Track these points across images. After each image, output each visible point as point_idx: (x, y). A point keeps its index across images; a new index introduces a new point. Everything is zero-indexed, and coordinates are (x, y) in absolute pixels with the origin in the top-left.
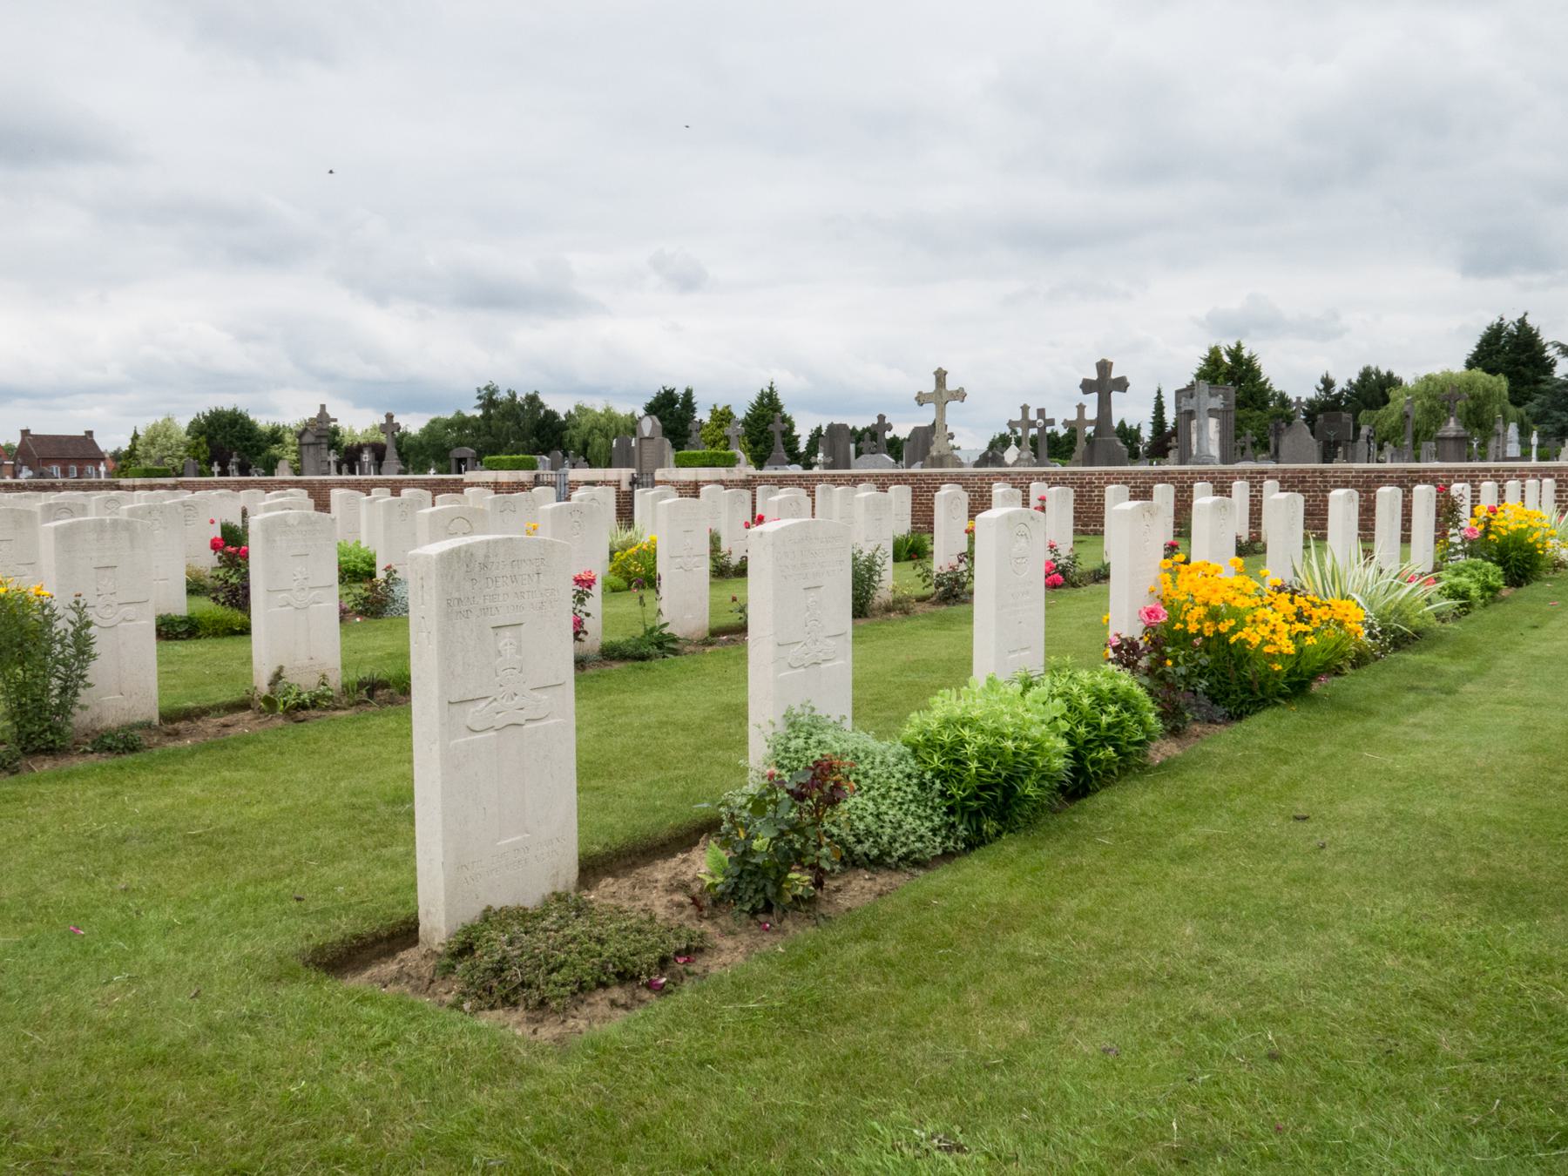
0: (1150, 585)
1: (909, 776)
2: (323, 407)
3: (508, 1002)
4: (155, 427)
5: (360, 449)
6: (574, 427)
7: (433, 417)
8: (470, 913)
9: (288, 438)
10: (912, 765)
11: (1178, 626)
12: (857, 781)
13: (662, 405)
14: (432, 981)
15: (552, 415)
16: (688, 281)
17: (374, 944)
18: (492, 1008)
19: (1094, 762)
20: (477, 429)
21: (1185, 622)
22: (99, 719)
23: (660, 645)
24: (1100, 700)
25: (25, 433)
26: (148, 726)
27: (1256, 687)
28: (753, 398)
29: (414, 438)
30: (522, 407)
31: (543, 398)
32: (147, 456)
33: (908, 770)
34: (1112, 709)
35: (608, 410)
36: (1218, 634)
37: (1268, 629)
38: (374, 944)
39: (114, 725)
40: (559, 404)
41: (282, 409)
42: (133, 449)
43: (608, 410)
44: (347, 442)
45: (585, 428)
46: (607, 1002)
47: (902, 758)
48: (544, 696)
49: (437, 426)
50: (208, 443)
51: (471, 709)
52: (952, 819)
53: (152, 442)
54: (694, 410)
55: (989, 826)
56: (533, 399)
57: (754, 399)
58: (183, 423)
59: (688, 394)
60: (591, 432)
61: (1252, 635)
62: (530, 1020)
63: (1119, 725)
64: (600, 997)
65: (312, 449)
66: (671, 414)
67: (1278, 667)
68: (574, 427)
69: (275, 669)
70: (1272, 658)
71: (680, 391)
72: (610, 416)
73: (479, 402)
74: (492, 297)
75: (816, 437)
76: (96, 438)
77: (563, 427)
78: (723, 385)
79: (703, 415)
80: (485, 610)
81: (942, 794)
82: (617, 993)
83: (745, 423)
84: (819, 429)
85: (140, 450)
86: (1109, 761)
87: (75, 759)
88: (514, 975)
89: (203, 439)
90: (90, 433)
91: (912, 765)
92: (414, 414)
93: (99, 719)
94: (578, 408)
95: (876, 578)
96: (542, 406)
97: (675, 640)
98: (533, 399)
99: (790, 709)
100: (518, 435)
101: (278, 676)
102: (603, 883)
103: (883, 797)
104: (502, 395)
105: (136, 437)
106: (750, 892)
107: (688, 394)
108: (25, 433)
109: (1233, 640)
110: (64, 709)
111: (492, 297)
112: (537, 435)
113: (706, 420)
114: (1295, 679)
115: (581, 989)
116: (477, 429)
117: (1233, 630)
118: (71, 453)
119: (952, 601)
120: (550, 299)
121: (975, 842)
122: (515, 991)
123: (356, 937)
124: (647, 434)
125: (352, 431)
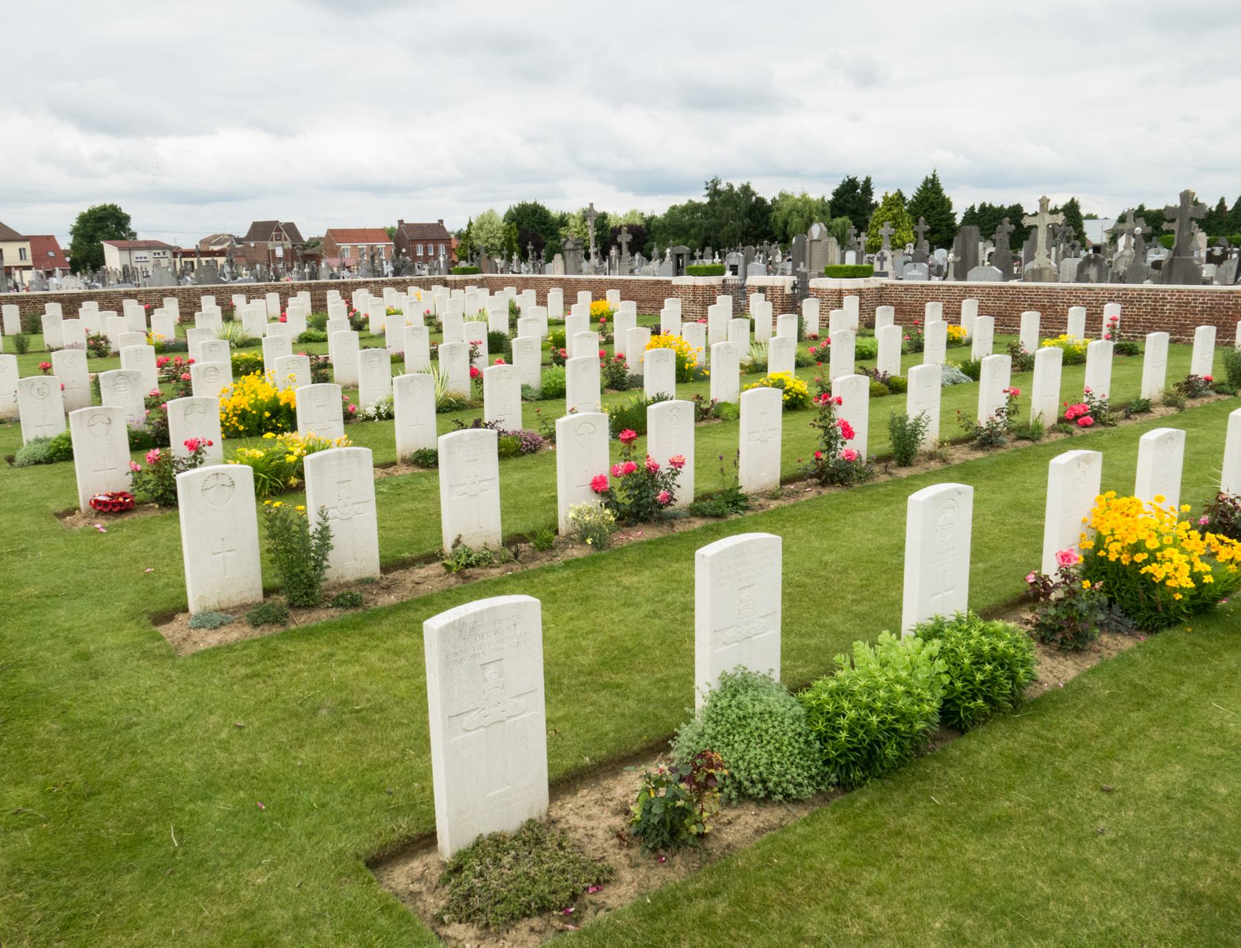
0: (1084, 516)
1: (800, 734)
2: (592, 205)
3: (469, 919)
7: (673, 204)
8: (467, 839)
9: (571, 223)
10: (802, 726)
12: (760, 736)
13: (846, 191)
15: (761, 201)
16: (865, 77)
18: (460, 922)
19: (966, 709)
20: (706, 213)
21: (1107, 551)
23: (735, 503)
24: (979, 659)
25: (401, 222)
26: (370, 581)
27: (1160, 608)
28: (919, 184)
31: (753, 187)
32: (478, 237)
33: (799, 730)
34: (988, 667)
35: (804, 196)
36: (1133, 563)
37: (1172, 567)
39: (352, 580)
40: (767, 191)
41: (565, 200)
42: (469, 232)
43: (804, 196)
45: (786, 210)
46: (527, 928)
47: (798, 718)
48: (522, 701)
49: (676, 212)
50: (518, 227)
51: (466, 718)
53: (481, 227)
54: (871, 194)
55: (857, 774)
56: (746, 189)
57: (919, 184)
60: (790, 213)
61: (1158, 572)
62: (478, 938)
63: (992, 681)
64: (524, 925)
65: (572, 254)
66: (853, 197)
67: (1178, 596)
69: (456, 537)
70: (1175, 590)
71: (861, 179)
72: (806, 201)
73: (706, 192)
74: (708, 100)
76: (445, 224)
77: (769, 209)
79: (877, 198)
80: (474, 656)
81: (821, 751)
82: (536, 922)
83: (912, 204)
84: (973, 208)
85: (473, 234)
86: (979, 708)
87: (321, 612)
88: (476, 902)
89: (514, 224)
90: (441, 221)
91: (802, 726)
92: (660, 197)
94: (781, 195)
95: (920, 437)
96: (754, 194)
97: (746, 499)
98: (746, 189)
100: (735, 225)
101: (458, 541)
103: (778, 750)
105: (470, 224)
106: (653, 836)
108: (401, 222)
109: (1143, 571)
110: (319, 566)
111: (708, 100)
112: (750, 217)
115: (512, 918)
116: (706, 213)
117: (1146, 563)
118: (430, 236)
120: (754, 99)
122: (474, 913)
123: (408, 837)
124: (815, 238)
125: (616, 216)
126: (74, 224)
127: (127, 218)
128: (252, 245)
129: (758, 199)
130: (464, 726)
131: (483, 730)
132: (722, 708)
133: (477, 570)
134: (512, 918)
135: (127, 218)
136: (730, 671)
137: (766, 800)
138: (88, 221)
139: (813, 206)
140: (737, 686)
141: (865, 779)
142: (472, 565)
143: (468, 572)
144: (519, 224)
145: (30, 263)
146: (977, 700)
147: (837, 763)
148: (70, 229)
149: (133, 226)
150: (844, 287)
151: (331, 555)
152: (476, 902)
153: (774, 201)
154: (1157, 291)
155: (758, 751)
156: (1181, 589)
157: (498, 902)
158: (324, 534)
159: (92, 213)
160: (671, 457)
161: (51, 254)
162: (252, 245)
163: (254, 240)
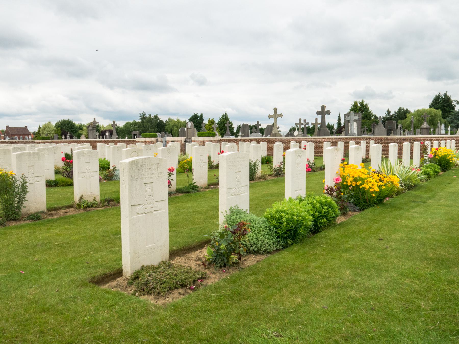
1: (266, 227)
2: (95, 119)
3: (149, 293)
4: (45, 125)
6: (168, 125)
7: (127, 122)
8: (138, 267)
9: (84, 128)
11: (345, 183)
14: (126, 287)
15: (162, 121)
17: (109, 276)
18: (144, 295)
19: (320, 223)
20: (140, 126)
21: (347, 182)
22: (29, 210)
23: (193, 189)
24: (322, 205)
25: (7, 127)
26: (43, 212)
27: (368, 201)
29: (121, 128)
30: (153, 119)
31: (159, 116)
32: (43, 133)
33: (266, 225)
34: (326, 207)
35: (178, 120)
36: (356, 185)
37: (371, 184)
38: (109, 276)
39: (33, 212)
41: (83, 120)
42: (39, 131)
43: (178, 120)
44: (102, 129)
45: (171, 125)
47: (264, 222)
48: (159, 204)
49: (128, 125)
50: (61, 130)
51: (138, 207)
52: (279, 240)
53: (44, 129)
54: (203, 120)
55: (290, 242)
56: (156, 117)
58: (54, 124)
59: (201, 115)
60: (173, 126)
61: (366, 186)
62: (155, 298)
63: (327, 212)
64: (176, 292)
65: (91, 131)
66: (197, 121)
67: (374, 195)
68: (168, 125)
70: (373, 192)
71: (199, 114)
72: (178, 121)
73: (140, 118)
76: (28, 128)
77: (165, 125)
78: (212, 112)
79: (206, 121)
80: (142, 179)
81: (276, 232)
82: (181, 290)
84: (240, 125)
85: (41, 132)
87: (22, 222)
88: (151, 285)
89: (59, 128)
90: (26, 127)
91: (267, 224)
94: (169, 119)
95: (256, 169)
96: (159, 119)
97: (198, 187)
98: (156, 117)
99: (231, 207)
101: (81, 198)
104: (147, 116)
105: (40, 128)
106: (220, 261)
107: (201, 115)
108: (7, 127)
109: (361, 187)
112: (157, 127)
115: (170, 289)
116: (140, 126)
117: (361, 184)
118: (21, 133)
119: (279, 176)
124: (189, 127)
129: (160, 121)
130: (137, 211)
131: (144, 214)
132: (233, 220)
133: (92, 208)
134: (170, 289)
136: (233, 208)
137: (256, 252)
139: (182, 124)
140: (235, 212)
141: (292, 244)
142: (89, 207)
143: (88, 209)
144: (62, 128)
146: (321, 224)
147: (282, 236)
150: (205, 140)
151: (27, 196)
152: (151, 285)
153: (166, 121)
154: (317, 138)
155: (251, 234)
156: (375, 192)
157: (162, 284)
158: (24, 188)
160: (169, 168)
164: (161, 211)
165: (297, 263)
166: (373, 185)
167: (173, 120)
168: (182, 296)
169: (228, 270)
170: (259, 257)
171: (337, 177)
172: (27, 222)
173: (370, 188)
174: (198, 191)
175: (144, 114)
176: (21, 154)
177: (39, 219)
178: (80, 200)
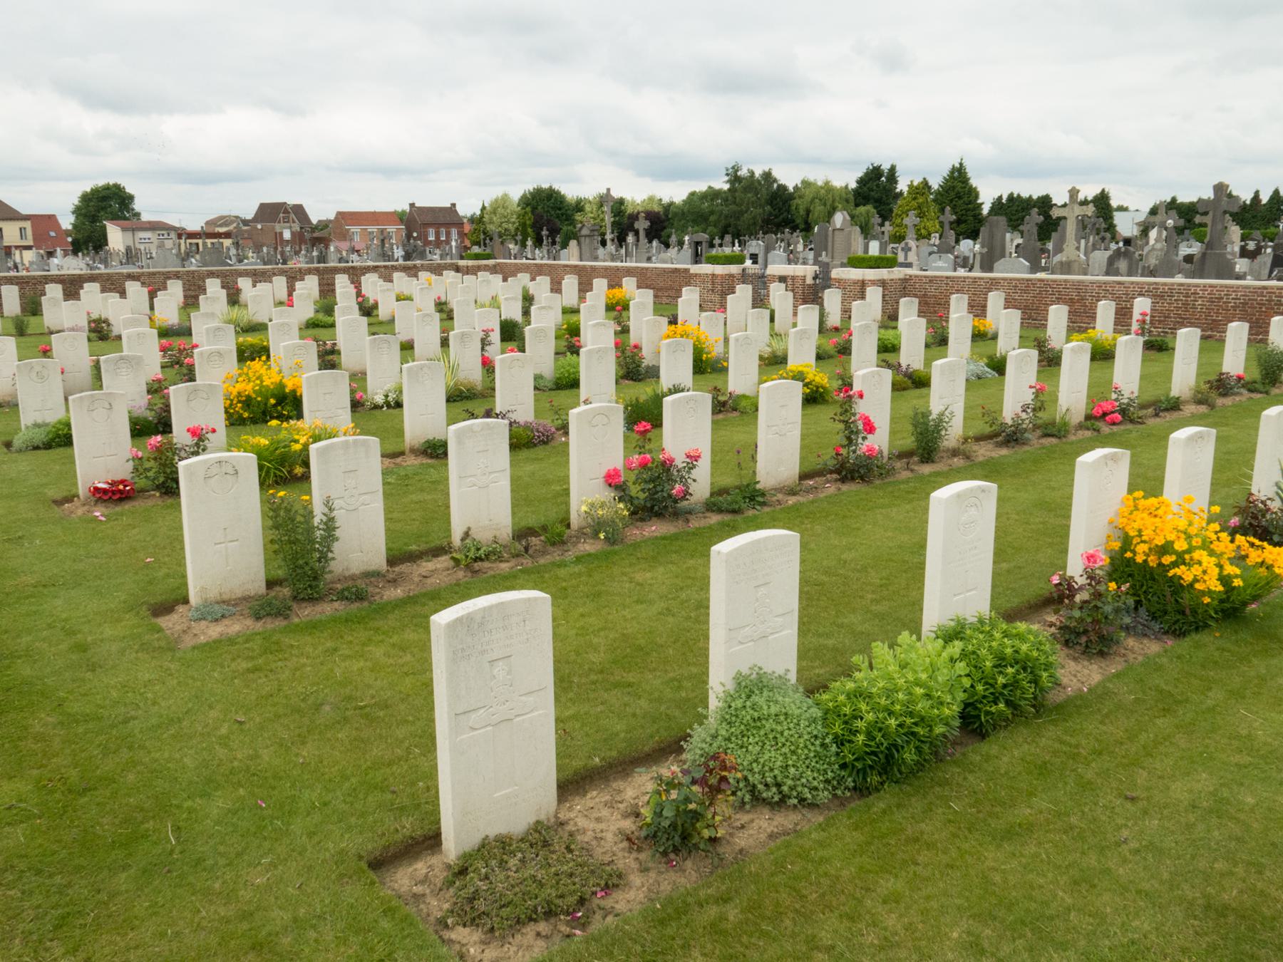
1: (816, 737)
3: (473, 922)
4: (496, 200)
5: (634, 217)
6: (800, 197)
8: (473, 841)
10: (818, 729)
11: (1128, 555)
12: (775, 738)
14: (441, 890)
15: (783, 188)
17: (423, 842)
19: (987, 713)
21: (1134, 553)
22: (347, 569)
23: (752, 499)
24: (1001, 662)
25: (412, 205)
26: (376, 574)
27: (1188, 612)
29: (677, 207)
30: (759, 181)
31: (775, 174)
32: (491, 222)
34: (1010, 670)
35: (827, 183)
36: (1160, 564)
37: (1200, 569)
38: (423, 842)
40: (789, 178)
41: (581, 184)
42: (482, 217)
43: (827, 183)
44: (630, 210)
46: (533, 933)
48: (531, 699)
50: (533, 212)
51: (473, 716)
52: (843, 773)
53: (494, 212)
54: (896, 182)
55: (874, 779)
56: (767, 176)
58: (516, 194)
59: (893, 169)
60: (812, 201)
61: (1186, 574)
62: (483, 942)
63: (1014, 684)
64: (530, 929)
65: (588, 240)
66: (878, 186)
67: (1207, 600)
68: (800, 197)
69: (465, 529)
70: (1203, 593)
71: (886, 167)
72: (828, 187)
73: (727, 178)
75: (998, 207)
76: (458, 208)
77: (791, 197)
78: (920, 164)
79: (902, 186)
80: (483, 652)
82: (543, 927)
83: (938, 193)
84: (1000, 197)
88: (481, 905)
89: (528, 209)
90: (454, 205)
91: (818, 729)
92: (679, 182)
93: (347, 569)
96: (775, 180)
97: (763, 495)
98: (767, 176)
99: (739, 673)
101: (467, 534)
102: (589, 796)
103: (793, 752)
104: (743, 172)
105: (484, 208)
106: (664, 840)
107: (893, 169)
108: (412, 205)
109: (1171, 573)
112: (771, 204)
113: (905, 189)
114: (1227, 605)
115: (518, 922)
117: (1175, 564)
118: (442, 220)
119: (1013, 444)
121: (862, 791)
124: (838, 226)
126: (76, 202)
127: (131, 198)
128: (259, 227)
134: (518, 922)
135: (131, 198)
136: (745, 671)
138: (90, 200)
141: (882, 784)
142: (481, 560)
143: (477, 566)
144: (534, 209)
145: (31, 243)
146: (996, 706)
148: (72, 208)
149: (137, 206)
150: (867, 278)
151: (336, 547)
152: (481, 905)
153: (796, 188)
155: (773, 754)
156: (1209, 593)
159: (95, 191)
161: (53, 234)
162: (259, 227)
163: (261, 222)
164: (536, 713)
165: (845, 873)
166: (1205, 572)
167: (815, 184)
168: (541, 942)
169: (685, 860)
170: (785, 820)
171: (1091, 552)
172: (336, 605)
173: (1196, 580)
174: (763, 504)
175: (736, 169)
176: (327, 448)
177: (360, 596)
178: (462, 540)
